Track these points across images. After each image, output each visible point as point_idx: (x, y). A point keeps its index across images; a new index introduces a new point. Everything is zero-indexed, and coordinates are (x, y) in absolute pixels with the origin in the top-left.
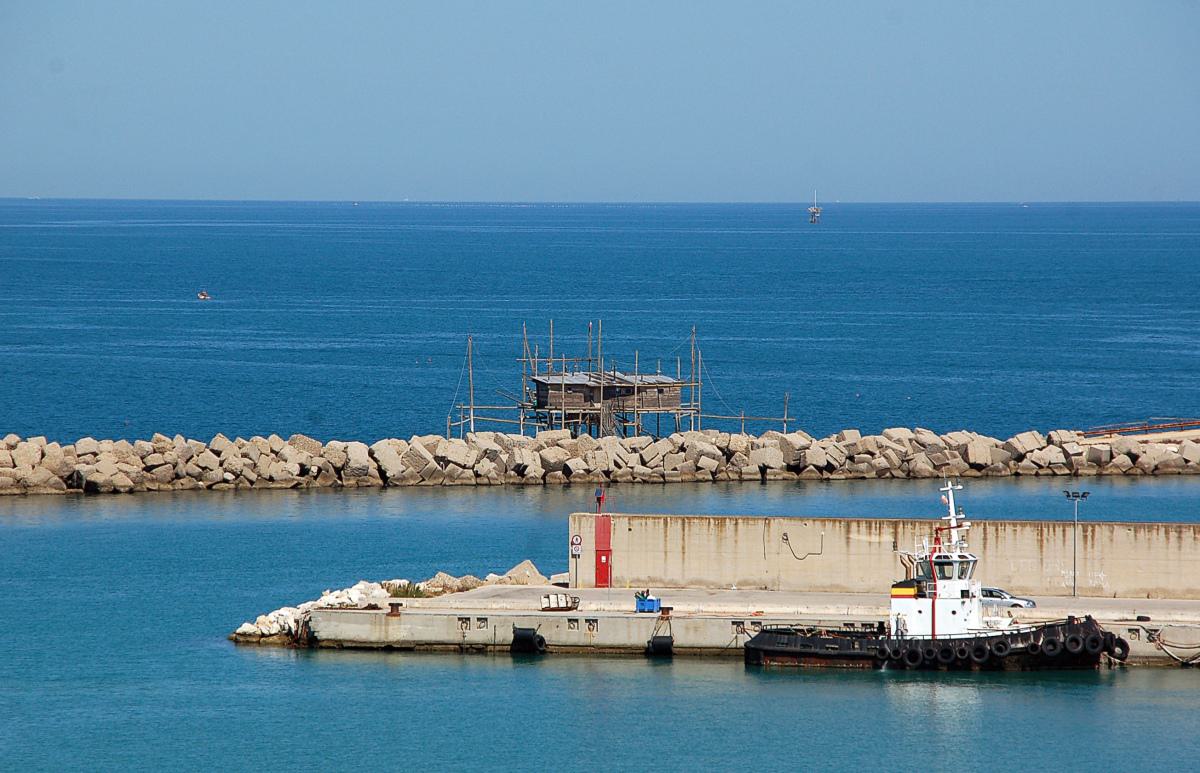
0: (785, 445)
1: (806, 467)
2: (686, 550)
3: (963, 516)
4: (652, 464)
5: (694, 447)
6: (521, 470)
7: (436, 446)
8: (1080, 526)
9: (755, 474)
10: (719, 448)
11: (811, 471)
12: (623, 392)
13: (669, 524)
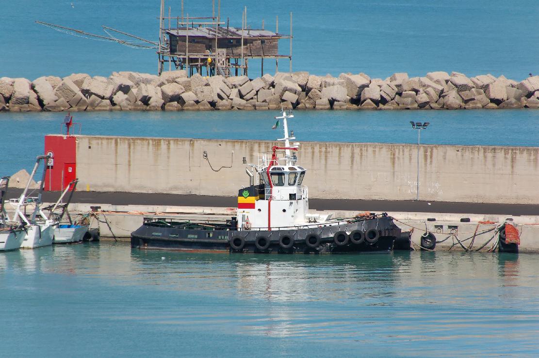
0: (350, 83)
1: (365, 100)
2: (131, 163)
3: (294, 138)
4: (248, 97)
5: (281, 84)
6: (146, 100)
7: (82, 82)
8: (422, 148)
9: (325, 105)
10: (299, 85)
11: (369, 104)
12: (234, 43)
13: (119, 144)
